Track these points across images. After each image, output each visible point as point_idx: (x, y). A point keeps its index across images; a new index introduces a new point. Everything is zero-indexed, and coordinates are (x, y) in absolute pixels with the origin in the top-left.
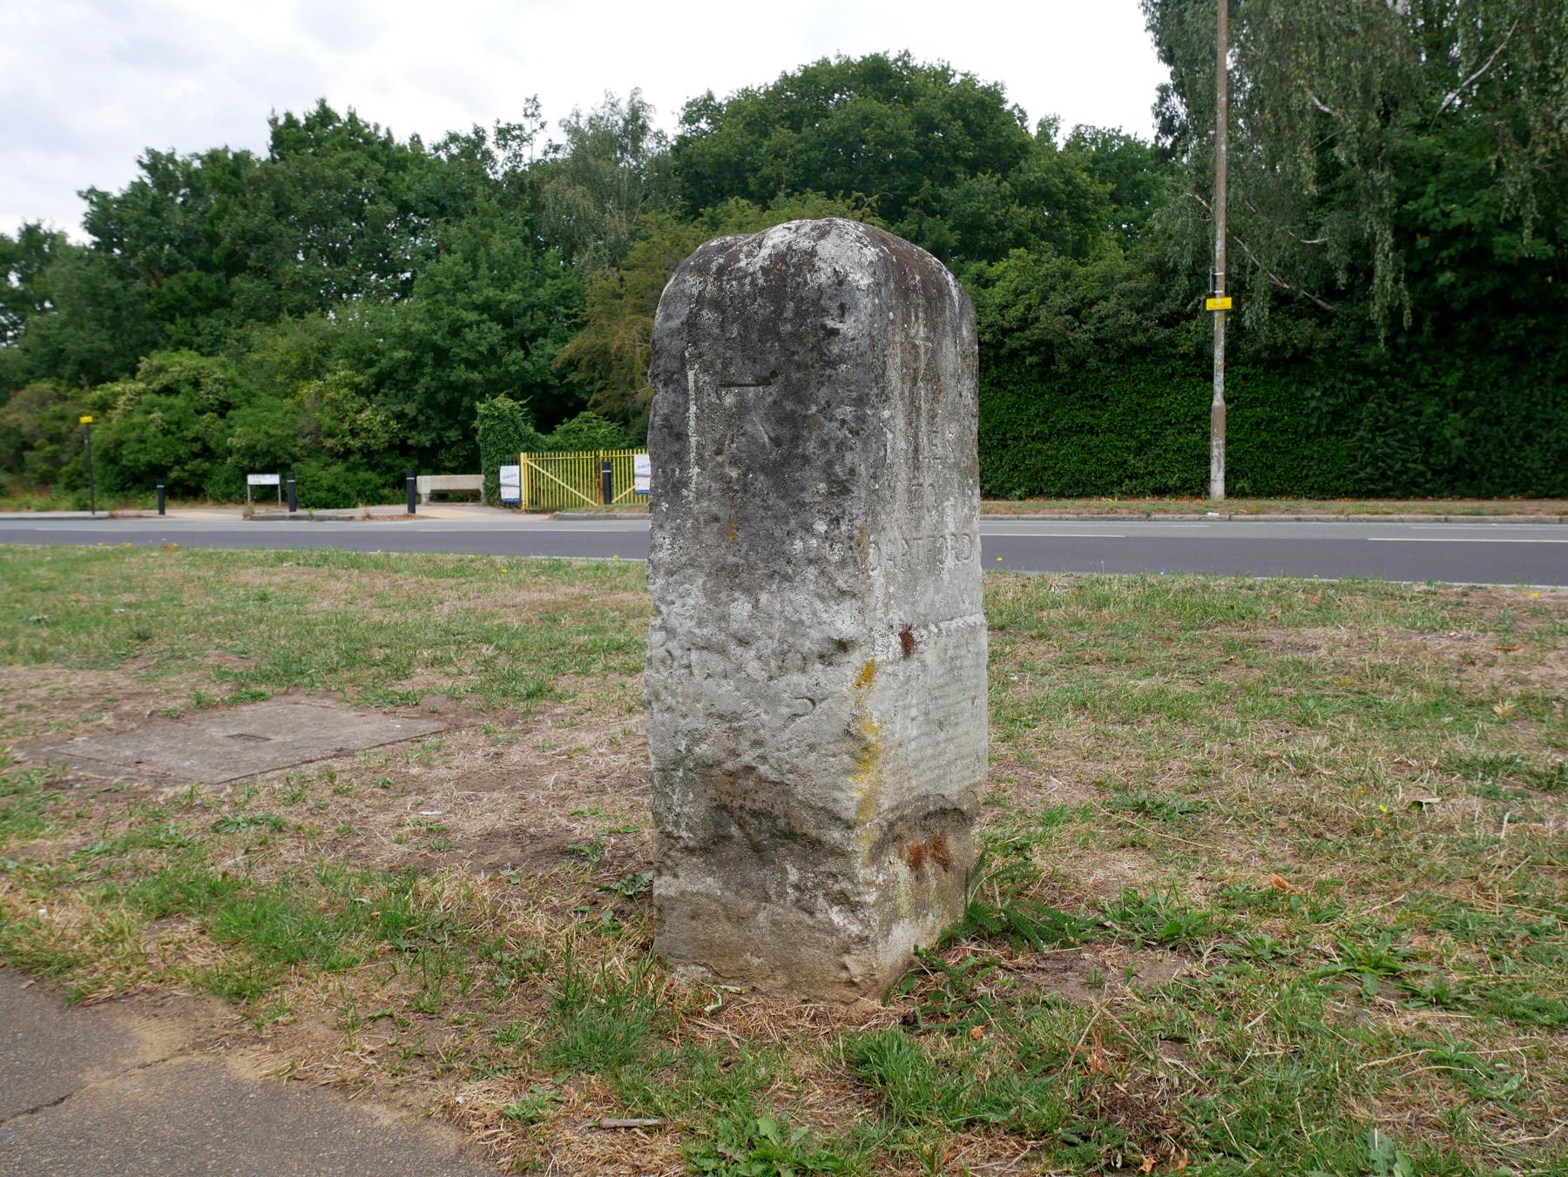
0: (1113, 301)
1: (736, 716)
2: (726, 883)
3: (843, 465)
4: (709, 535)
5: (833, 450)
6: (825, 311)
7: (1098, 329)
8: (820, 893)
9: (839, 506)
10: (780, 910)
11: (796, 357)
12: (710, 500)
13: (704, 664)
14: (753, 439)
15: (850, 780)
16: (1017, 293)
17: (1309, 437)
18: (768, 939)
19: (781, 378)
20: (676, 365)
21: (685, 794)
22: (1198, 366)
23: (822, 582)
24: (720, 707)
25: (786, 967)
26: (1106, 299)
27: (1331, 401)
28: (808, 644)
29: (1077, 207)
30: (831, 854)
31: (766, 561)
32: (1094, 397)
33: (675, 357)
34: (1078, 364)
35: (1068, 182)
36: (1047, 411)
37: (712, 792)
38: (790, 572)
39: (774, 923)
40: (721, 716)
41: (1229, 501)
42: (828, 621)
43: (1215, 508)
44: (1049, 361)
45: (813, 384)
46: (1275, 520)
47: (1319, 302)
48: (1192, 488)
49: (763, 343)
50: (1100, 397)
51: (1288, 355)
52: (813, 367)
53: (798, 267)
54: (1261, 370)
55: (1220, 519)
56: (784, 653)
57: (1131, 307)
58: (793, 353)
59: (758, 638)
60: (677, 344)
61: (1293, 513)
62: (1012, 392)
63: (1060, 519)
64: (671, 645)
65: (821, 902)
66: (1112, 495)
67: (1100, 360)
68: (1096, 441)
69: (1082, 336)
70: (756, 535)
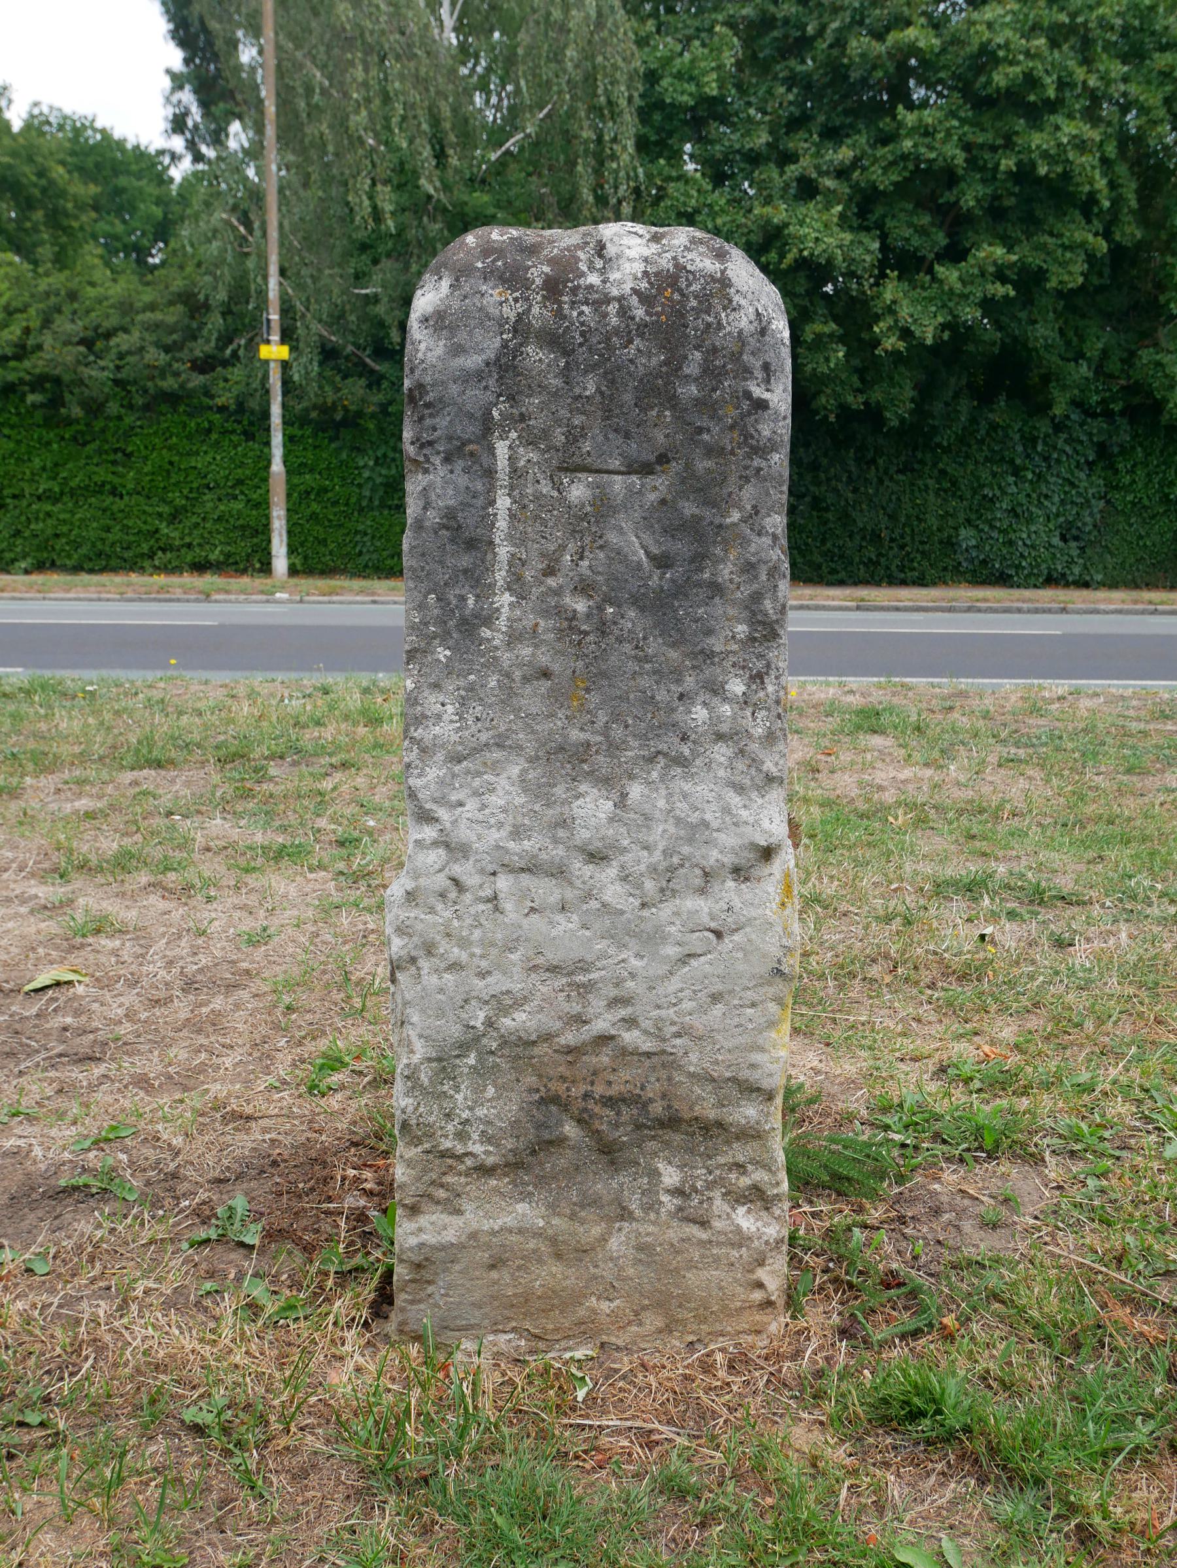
0: (136, 334)
1: (583, 966)
2: (553, 1208)
3: (775, 599)
4: (532, 698)
5: (764, 578)
6: (746, 372)
7: (118, 368)
8: (717, 1194)
9: (760, 656)
10: (651, 1229)
11: (706, 437)
12: (536, 646)
13: (525, 894)
14: (619, 555)
15: (773, 1035)
17: (361, 510)
18: (631, 1271)
20: (471, 430)
21: (479, 1090)
22: (239, 422)
23: (740, 765)
24: (552, 956)
25: (661, 1304)
26: (126, 330)
27: (384, 472)
28: (715, 854)
29: (55, 211)
30: (738, 1138)
31: (644, 737)
32: (116, 451)
33: (471, 416)
34: (94, 408)
35: (41, 174)
36: (56, 465)
37: (531, 1080)
38: (687, 752)
39: (640, 1248)
40: (554, 969)
41: (294, 581)
42: (751, 820)
43: (282, 588)
44: (56, 402)
45: (733, 479)
46: (350, 603)
47: (368, 360)
48: (236, 563)
49: (644, 410)
50: (124, 452)
51: (338, 416)
52: (732, 453)
53: (705, 299)
54: (308, 431)
55: (290, 601)
56: (672, 869)
57: (158, 344)
58: (700, 430)
59: (624, 850)
60: (475, 398)
61: (368, 595)
62: (9, 437)
63: (100, 600)
64: (457, 869)
65: (719, 1204)
66: (142, 570)
67: (122, 406)
68: (120, 504)
69: (99, 374)
70: (622, 698)
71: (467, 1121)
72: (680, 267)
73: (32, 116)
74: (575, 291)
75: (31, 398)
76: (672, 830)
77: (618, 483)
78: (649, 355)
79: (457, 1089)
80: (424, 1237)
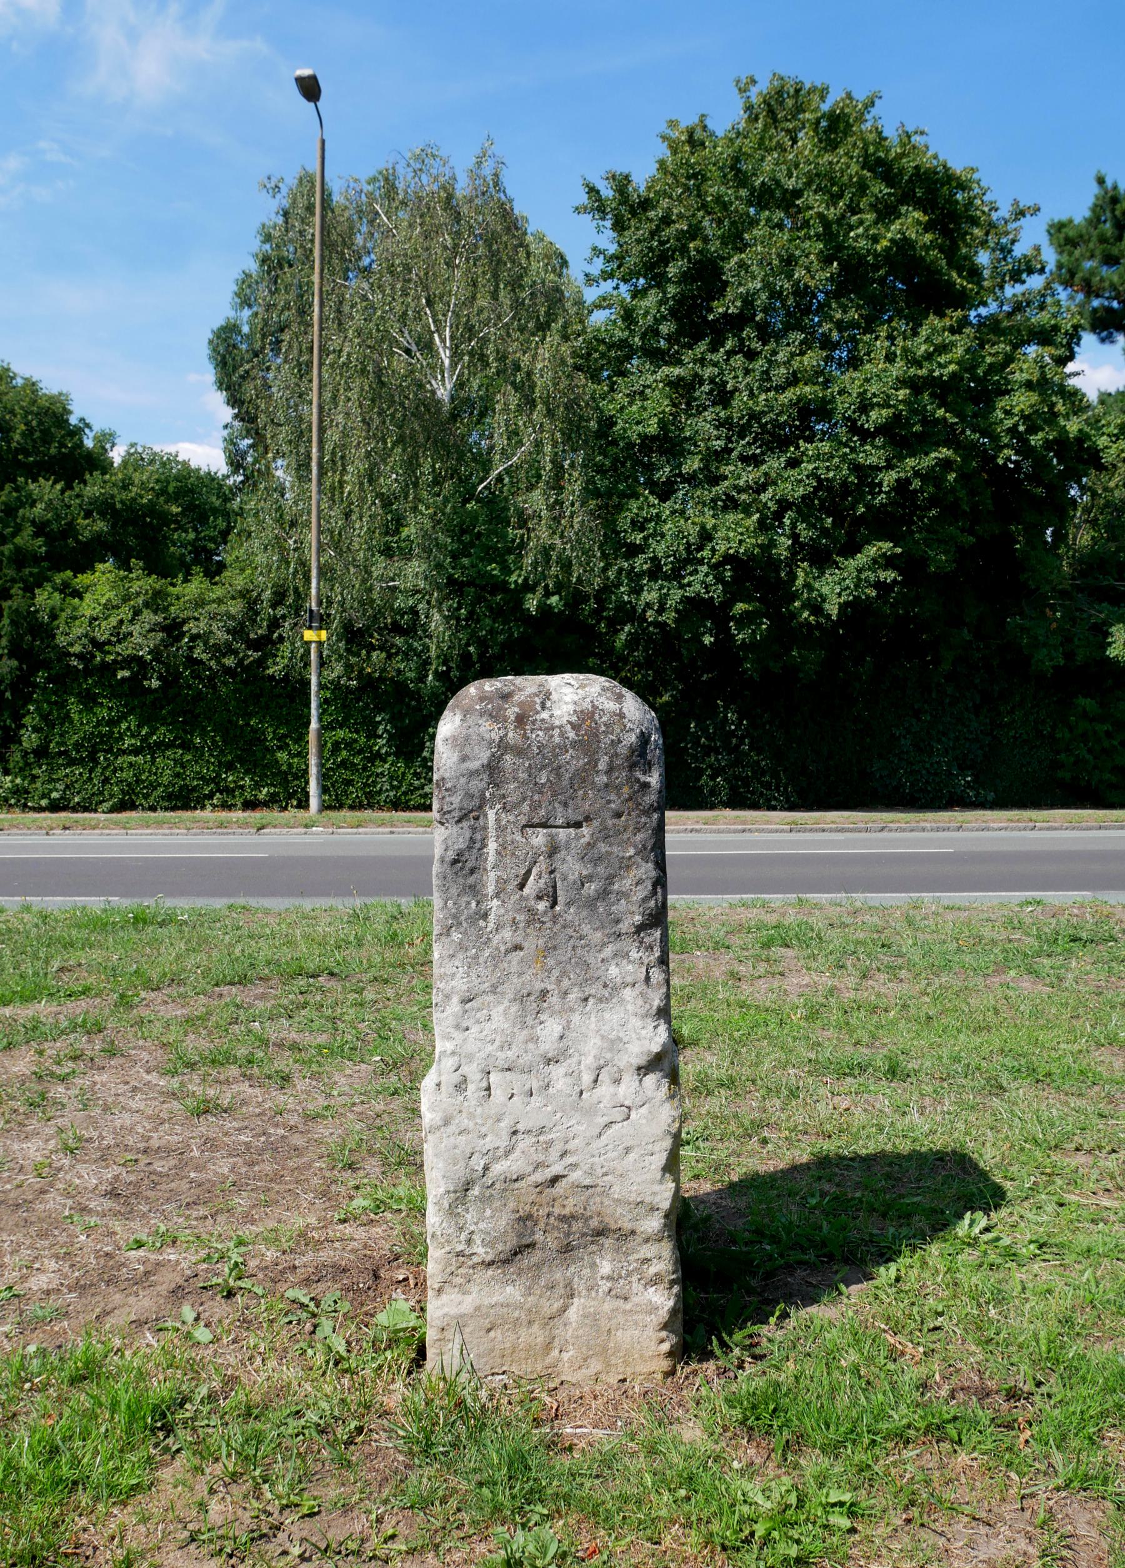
16: (109, 607)
19: (596, 823)
65: (637, 1287)
71: (472, 1233)
72: (595, 707)
73: (130, 454)
74: (534, 722)
75: (120, 675)
76: (599, 1043)
77: (562, 834)
78: (578, 759)
79: (467, 1210)
80: (446, 1310)
